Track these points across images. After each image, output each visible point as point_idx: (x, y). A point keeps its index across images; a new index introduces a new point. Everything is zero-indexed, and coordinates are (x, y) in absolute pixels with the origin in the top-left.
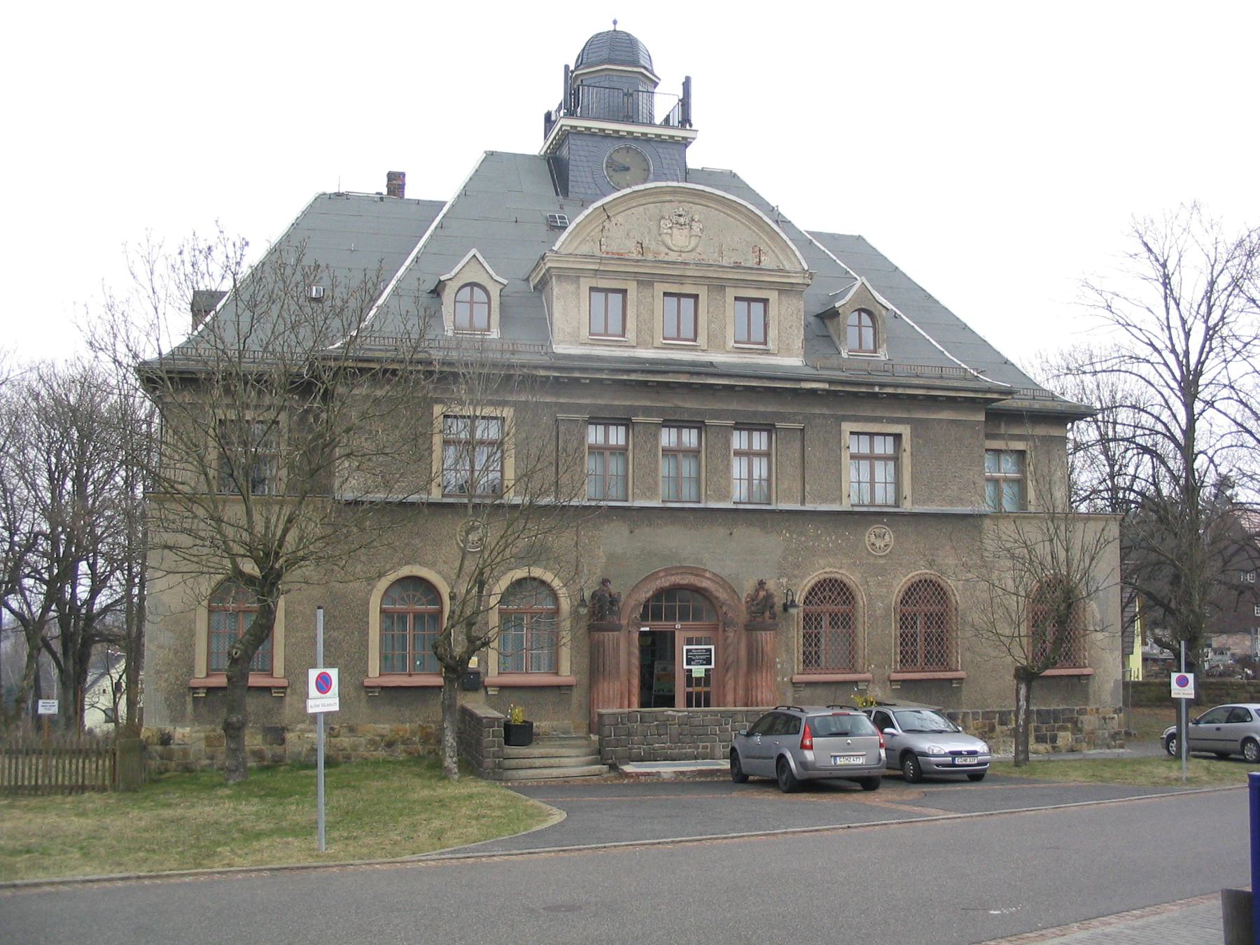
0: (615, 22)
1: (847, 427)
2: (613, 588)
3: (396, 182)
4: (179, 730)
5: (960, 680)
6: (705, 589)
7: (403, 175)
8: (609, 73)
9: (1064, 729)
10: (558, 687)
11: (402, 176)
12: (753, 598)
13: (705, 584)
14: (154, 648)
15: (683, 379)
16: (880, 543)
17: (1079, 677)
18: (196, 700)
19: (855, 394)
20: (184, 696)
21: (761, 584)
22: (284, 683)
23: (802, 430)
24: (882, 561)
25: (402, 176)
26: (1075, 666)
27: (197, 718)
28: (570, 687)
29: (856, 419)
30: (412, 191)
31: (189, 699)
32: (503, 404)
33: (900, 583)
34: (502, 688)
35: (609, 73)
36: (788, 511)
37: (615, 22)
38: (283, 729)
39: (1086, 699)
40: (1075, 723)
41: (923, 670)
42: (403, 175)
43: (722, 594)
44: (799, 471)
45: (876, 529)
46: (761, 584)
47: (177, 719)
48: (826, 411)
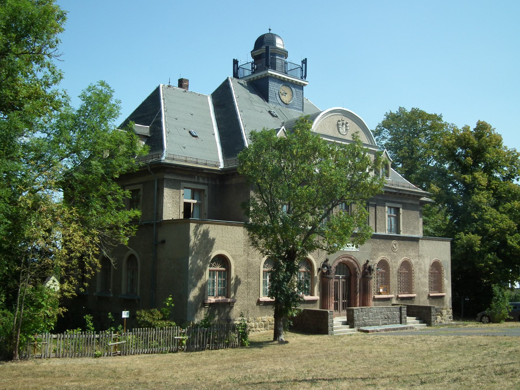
2: (370, 264)
5: (414, 297)
28: (317, 300)
33: (400, 261)
37: (270, 30)
39: (443, 304)
40: (441, 313)
41: (404, 294)
44: (374, 220)
45: (394, 242)
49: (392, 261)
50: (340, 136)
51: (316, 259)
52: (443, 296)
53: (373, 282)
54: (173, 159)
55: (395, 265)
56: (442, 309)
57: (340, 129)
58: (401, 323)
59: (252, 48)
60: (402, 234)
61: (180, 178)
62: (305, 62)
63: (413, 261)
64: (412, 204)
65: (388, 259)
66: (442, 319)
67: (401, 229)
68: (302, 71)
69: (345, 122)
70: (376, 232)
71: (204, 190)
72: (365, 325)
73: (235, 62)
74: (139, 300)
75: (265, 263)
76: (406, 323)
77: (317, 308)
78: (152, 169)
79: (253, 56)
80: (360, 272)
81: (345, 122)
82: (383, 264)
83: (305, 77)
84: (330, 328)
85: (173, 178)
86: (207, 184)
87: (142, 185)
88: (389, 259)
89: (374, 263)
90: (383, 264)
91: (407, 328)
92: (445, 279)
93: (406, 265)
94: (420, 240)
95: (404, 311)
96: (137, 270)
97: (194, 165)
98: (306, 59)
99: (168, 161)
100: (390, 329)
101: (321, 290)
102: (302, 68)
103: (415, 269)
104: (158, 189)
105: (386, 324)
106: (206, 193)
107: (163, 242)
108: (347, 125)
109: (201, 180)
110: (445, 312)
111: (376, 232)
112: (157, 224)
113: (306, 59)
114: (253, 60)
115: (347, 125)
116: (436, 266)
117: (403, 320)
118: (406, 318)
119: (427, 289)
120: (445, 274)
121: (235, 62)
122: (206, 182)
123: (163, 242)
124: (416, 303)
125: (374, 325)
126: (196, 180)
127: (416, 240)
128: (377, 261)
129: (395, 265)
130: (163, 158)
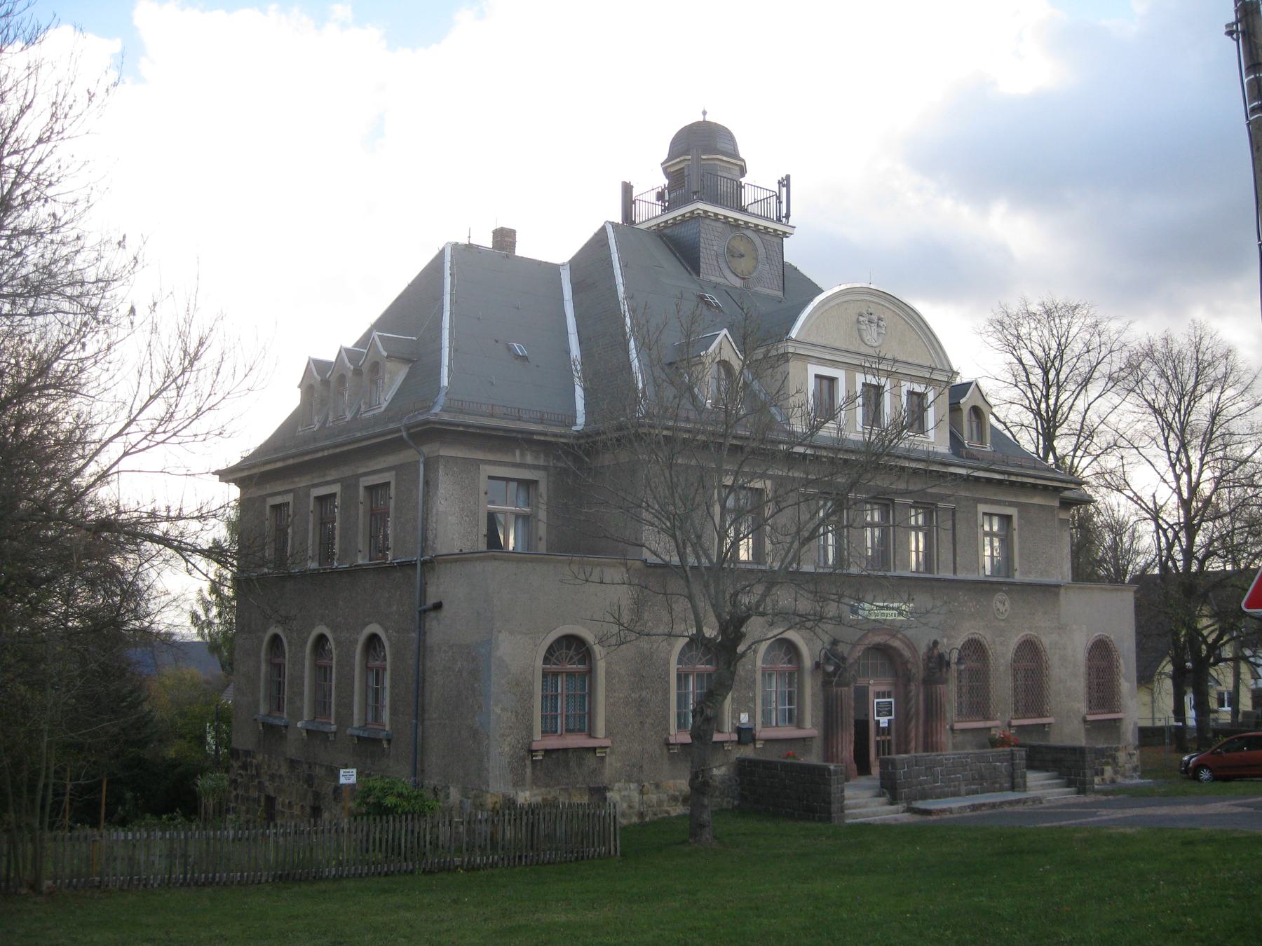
0: (704, 113)
1: (982, 508)
2: (941, 649)
3: (504, 238)
4: (521, 794)
6: (894, 649)
7: (514, 232)
8: (702, 159)
9: (1107, 764)
10: (804, 739)
11: (511, 233)
12: (929, 658)
13: (896, 644)
14: (499, 711)
15: (501, 433)
16: (1002, 609)
17: (1115, 720)
18: (534, 762)
19: (1023, 485)
20: (524, 759)
21: (935, 643)
22: (607, 743)
23: (954, 511)
24: (1002, 624)
25: (511, 233)
26: (1040, 716)
27: (535, 782)
28: (811, 738)
29: (986, 501)
30: (523, 249)
31: (528, 762)
32: (763, 476)
33: (1014, 641)
34: (548, 752)
35: (702, 159)
36: (969, 582)
37: (704, 113)
38: (606, 789)
39: (1119, 739)
41: (1024, 717)
42: (514, 232)
43: (907, 653)
45: (1000, 596)
46: (935, 643)
47: (519, 783)
48: (968, 494)
49: (994, 642)
50: (863, 349)
51: (809, 642)
52: (1120, 719)
53: (950, 692)
54: (461, 412)
55: (1003, 652)
56: (1117, 749)
57: (864, 334)
58: (1013, 788)
59: (665, 156)
60: (1018, 577)
61: (479, 455)
62: (785, 182)
63: (1046, 641)
64: (1041, 506)
65: (986, 636)
66: (1116, 772)
67: (1016, 565)
68: (780, 202)
69: (874, 318)
70: (955, 572)
71: (536, 482)
72: (924, 797)
73: (627, 189)
74: (389, 741)
75: (682, 653)
76: (1024, 787)
77: (813, 758)
78: (411, 436)
79: (668, 174)
80: (918, 671)
81: (874, 318)
82: (975, 648)
83: (788, 216)
84: (834, 807)
85: (460, 455)
86: (545, 468)
87: (393, 473)
88: (988, 637)
89: (952, 644)
90: (975, 648)
91: (1025, 802)
92: (1122, 680)
93: (1030, 650)
94: (1062, 591)
95: (1020, 761)
96: (302, 694)
97: (511, 425)
98: (788, 177)
99: (446, 417)
100: (984, 805)
101: (821, 714)
102: (779, 198)
103: (1053, 659)
104: (427, 483)
105: (975, 792)
106: (543, 488)
107: (438, 606)
108: (881, 323)
109: (529, 459)
110: (1122, 756)
111: (955, 572)
112: (424, 563)
113: (788, 177)
114: (666, 182)
115: (881, 323)
116: (1101, 651)
117: (1019, 780)
118: (1024, 777)
119: (1081, 706)
120: (1123, 669)
121: (627, 189)
122: (542, 462)
123: (438, 606)
124: (1055, 740)
125: (946, 795)
126: (518, 459)
127: (1051, 590)
128: (959, 642)
129: (1003, 652)
130: (437, 409)
